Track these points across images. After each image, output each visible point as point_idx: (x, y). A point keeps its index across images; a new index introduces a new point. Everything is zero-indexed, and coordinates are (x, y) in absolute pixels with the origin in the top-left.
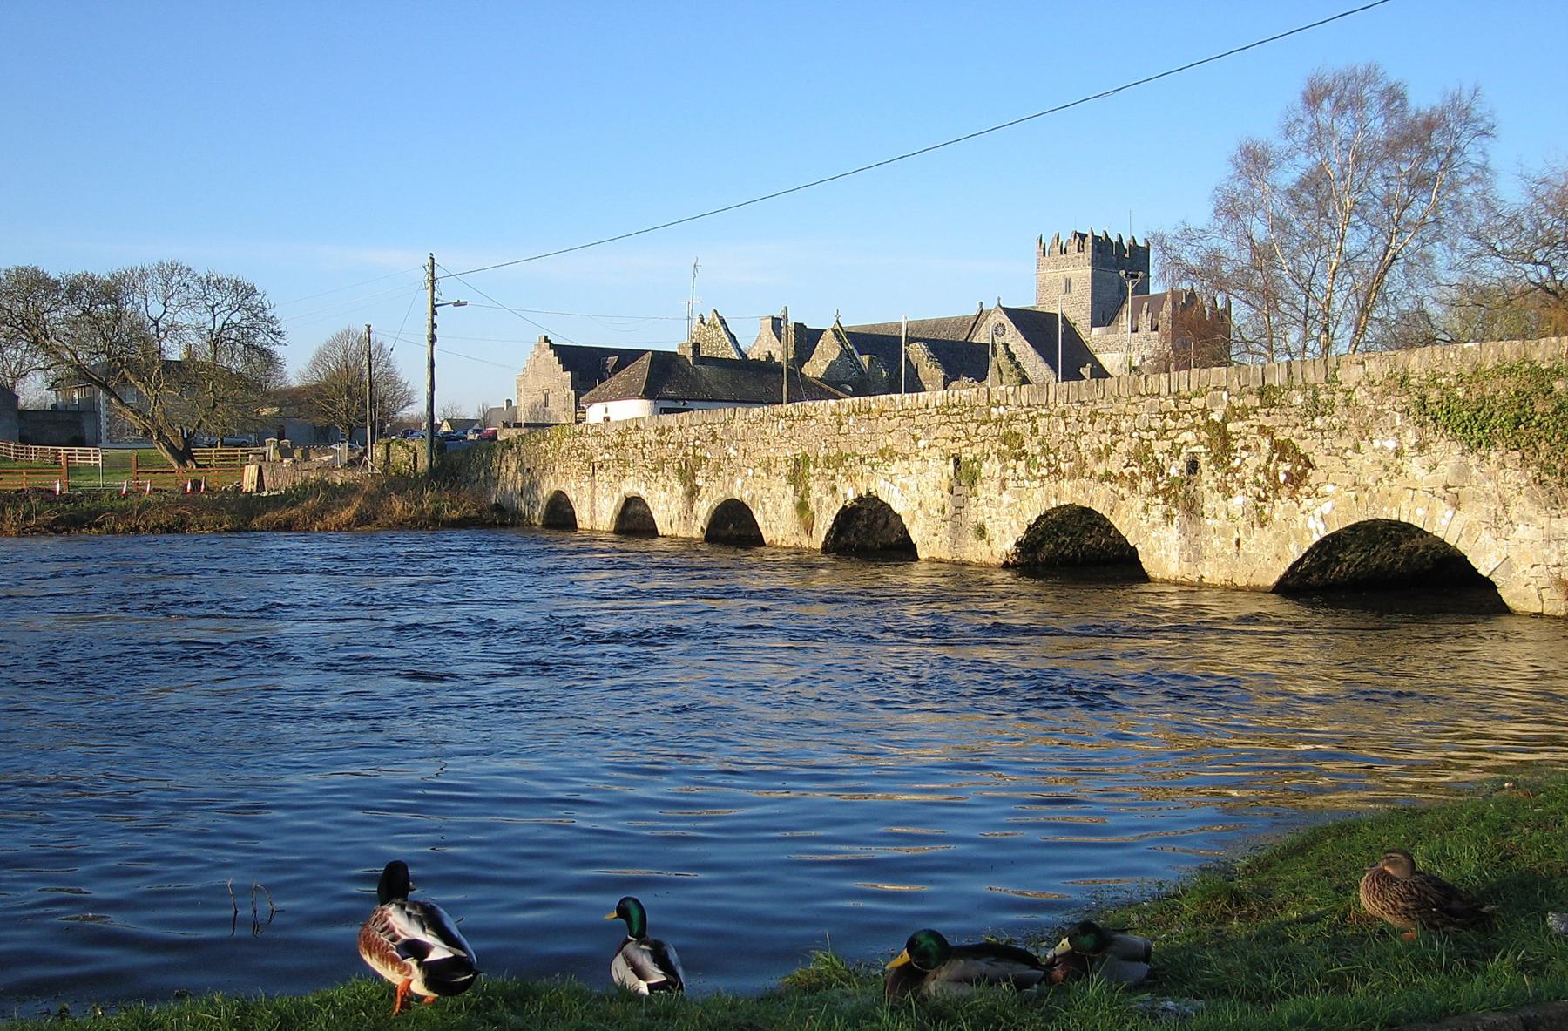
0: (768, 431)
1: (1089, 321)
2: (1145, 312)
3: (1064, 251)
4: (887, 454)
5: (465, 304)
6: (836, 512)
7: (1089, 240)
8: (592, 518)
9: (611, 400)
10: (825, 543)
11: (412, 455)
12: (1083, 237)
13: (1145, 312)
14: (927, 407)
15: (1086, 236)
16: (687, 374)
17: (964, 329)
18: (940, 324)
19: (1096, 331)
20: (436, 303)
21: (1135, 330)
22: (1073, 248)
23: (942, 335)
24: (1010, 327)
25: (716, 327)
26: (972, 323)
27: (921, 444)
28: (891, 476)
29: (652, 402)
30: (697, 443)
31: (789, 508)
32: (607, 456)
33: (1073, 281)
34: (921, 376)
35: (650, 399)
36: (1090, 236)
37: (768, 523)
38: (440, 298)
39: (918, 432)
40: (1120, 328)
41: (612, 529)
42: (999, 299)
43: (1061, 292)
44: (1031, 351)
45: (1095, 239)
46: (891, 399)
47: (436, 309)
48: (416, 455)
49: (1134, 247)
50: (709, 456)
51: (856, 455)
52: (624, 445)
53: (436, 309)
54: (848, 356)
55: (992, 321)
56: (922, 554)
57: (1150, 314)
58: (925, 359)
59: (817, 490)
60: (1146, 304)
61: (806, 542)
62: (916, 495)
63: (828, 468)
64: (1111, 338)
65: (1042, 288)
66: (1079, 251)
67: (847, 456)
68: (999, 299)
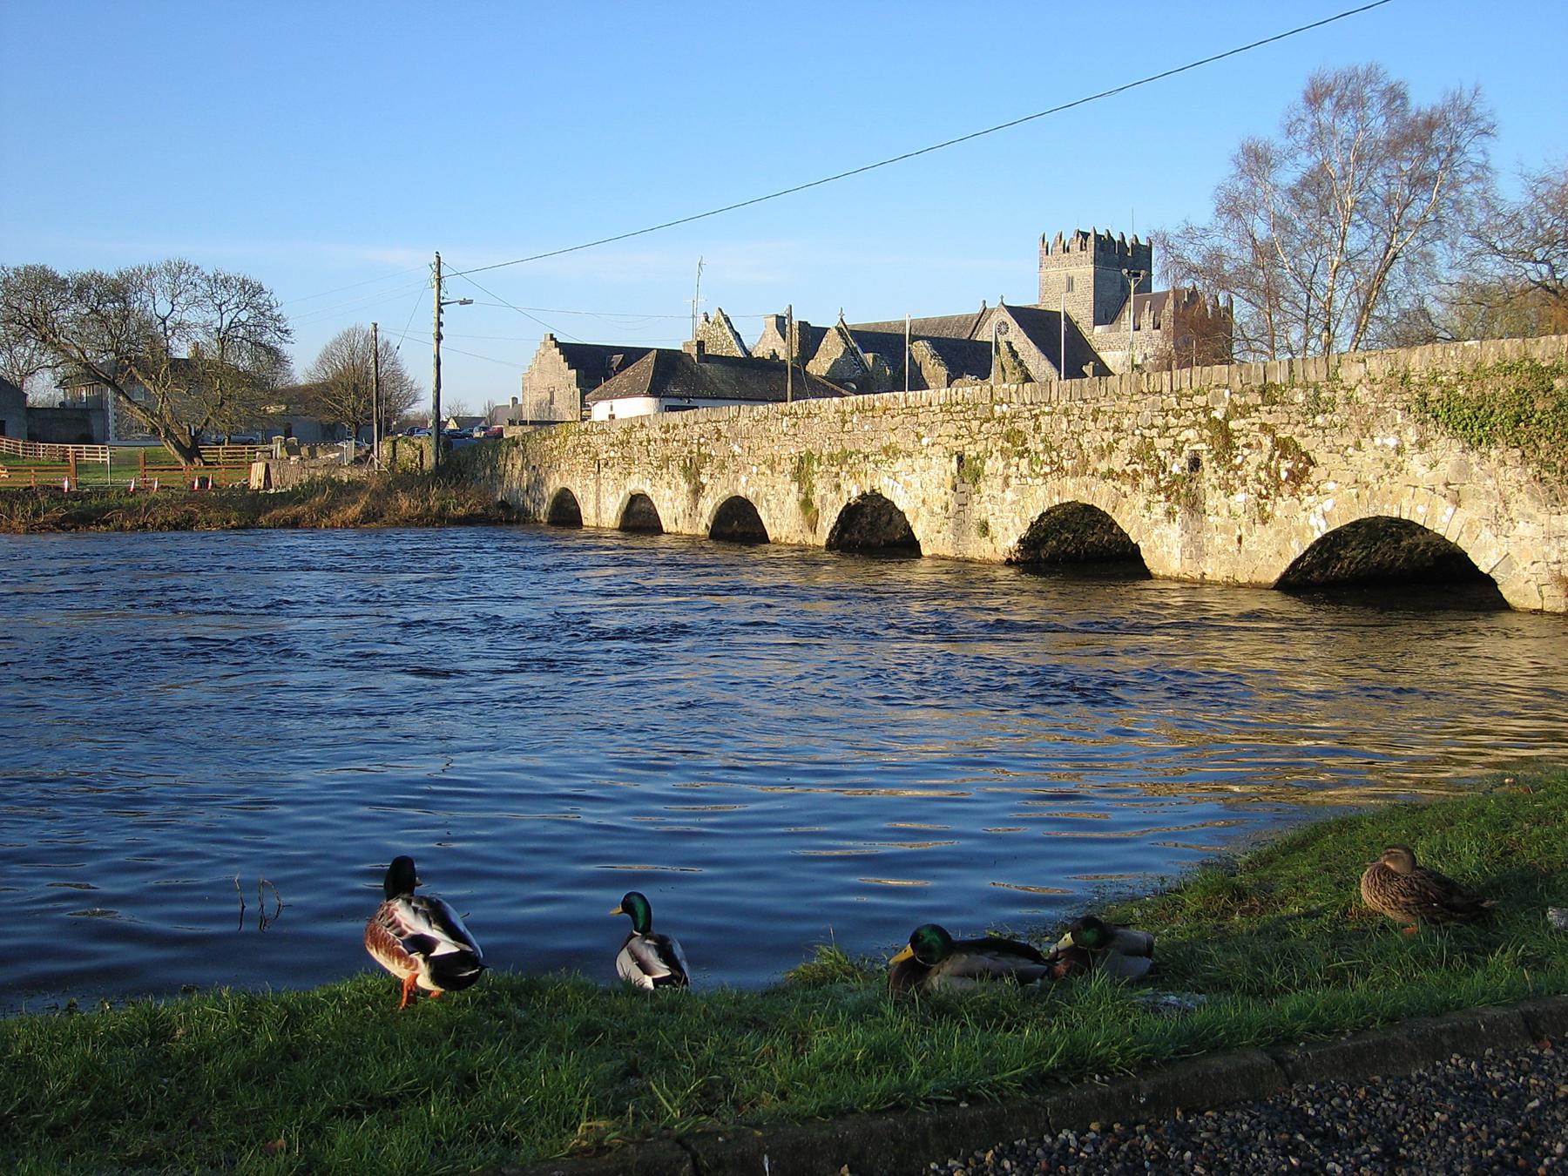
0: (772, 429)
1: (1091, 320)
2: (1147, 310)
3: (1066, 250)
4: (891, 452)
5: (471, 302)
6: (840, 509)
7: (1091, 238)
8: (597, 516)
9: (616, 398)
10: (829, 540)
11: (418, 452)
12: (1086, 235)
13: (1147, 310)
14: (930, 405)
15: (1089, 234)
16: (692, 372)
17: (967, 328)
18: (944, 322)
19: (1098, 329)
20: (442, 301)
21: (1137, 329)
22: (1075, 246)
23: (946, 334)
24: (1013, 325)
25: (720, 326)
26: (975, 321)
27: (925, 441)
28: (894, 473)
29: (657, 399)
30: (702, 440)
31: (792, 505)
32: (612, 454)
33: (1075, 279)
34: (925, 374)
35: (655, 396)
36: (1093, 235)
37: (772, 520)
38: (446, 296)
39: (921, 430)
40: (1122, 326)
41: (617, 526)
42: (1002, 297)
43: (1065, 289)
44: (1034, 349)
45: (1098, 237)
46: (895, 397)
47: (442, 307)
48: (422, 453)
49: (1137, 246)
50: (713, 453)
51: (860, 452)
52: (629, 443)
53: (442, 307)
54: (852, 355)
55: (995, 319)
56: (926, 551)
57: (1153, 312)
58: (929, 357)
59: (821, 488)
60: (1149, 302)
61: (810, 539)
62: (920, 492)
63: (832, 465)
64: (1113, 336)
65: (1045, 286)
66: (1081, 249)
67: (851, 454)
68: (1002, 297)
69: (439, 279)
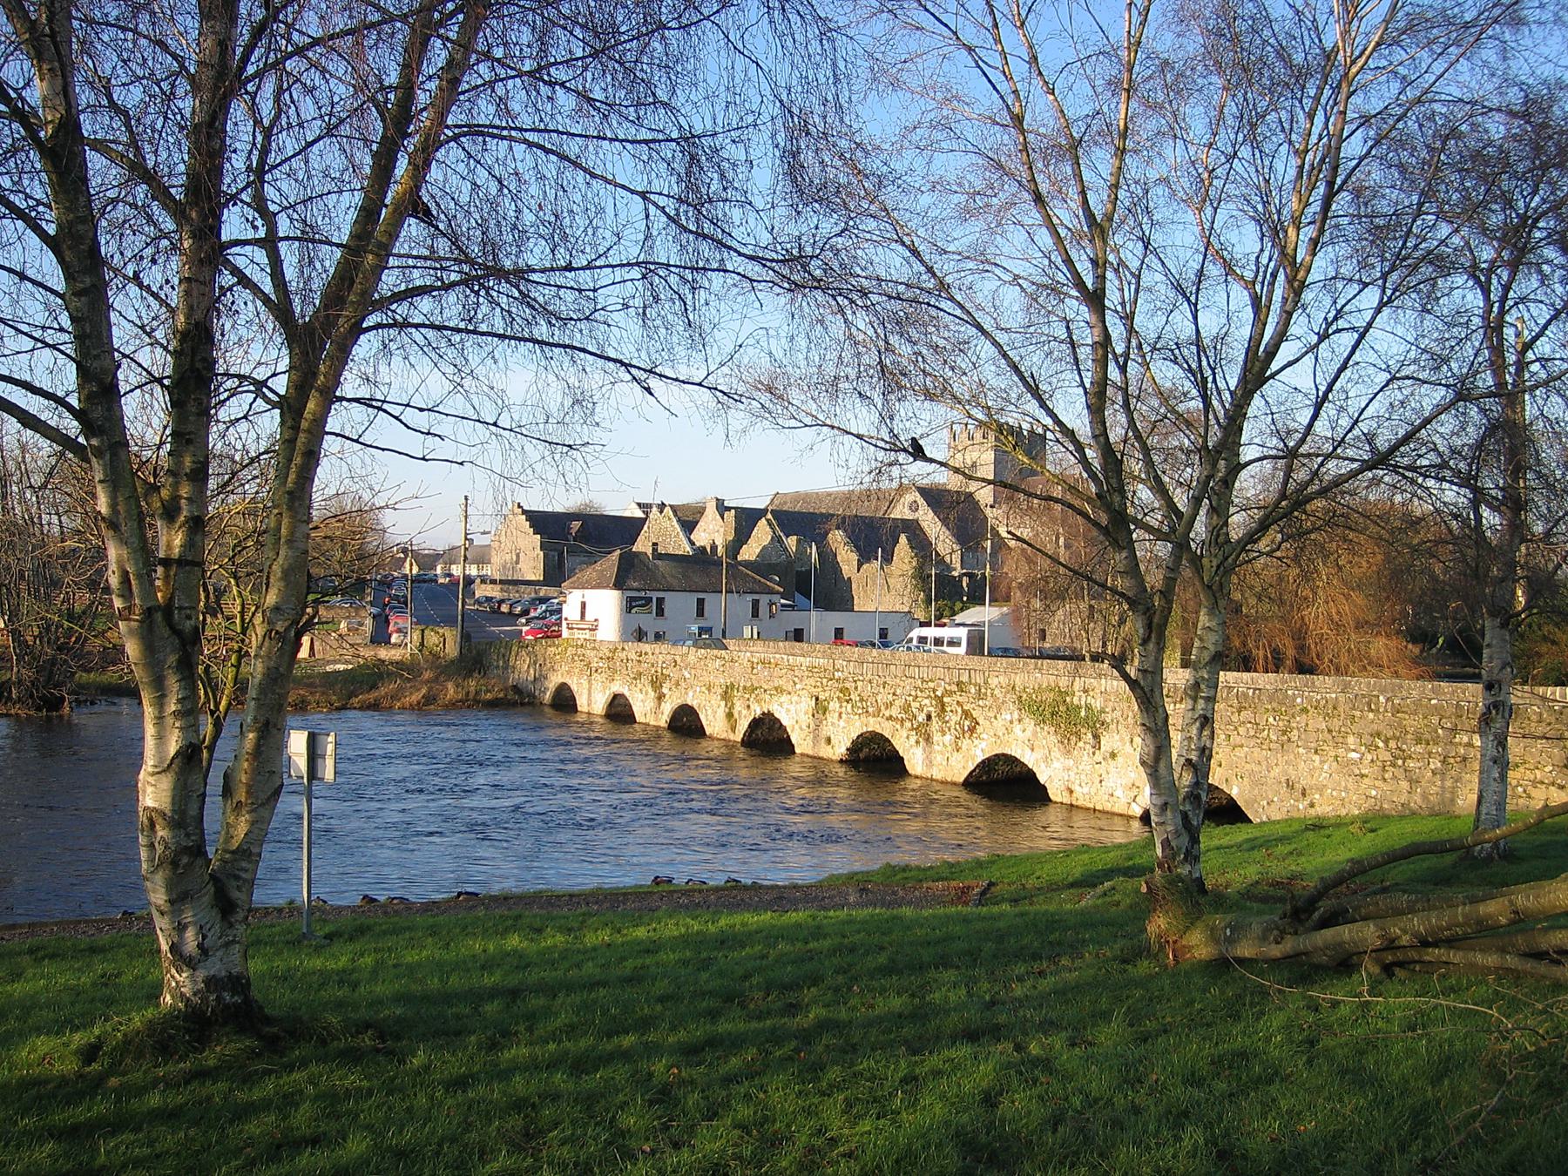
4: (779, 690)
34: (839, 558)
56: (798, 750)
69: (466, 517)
